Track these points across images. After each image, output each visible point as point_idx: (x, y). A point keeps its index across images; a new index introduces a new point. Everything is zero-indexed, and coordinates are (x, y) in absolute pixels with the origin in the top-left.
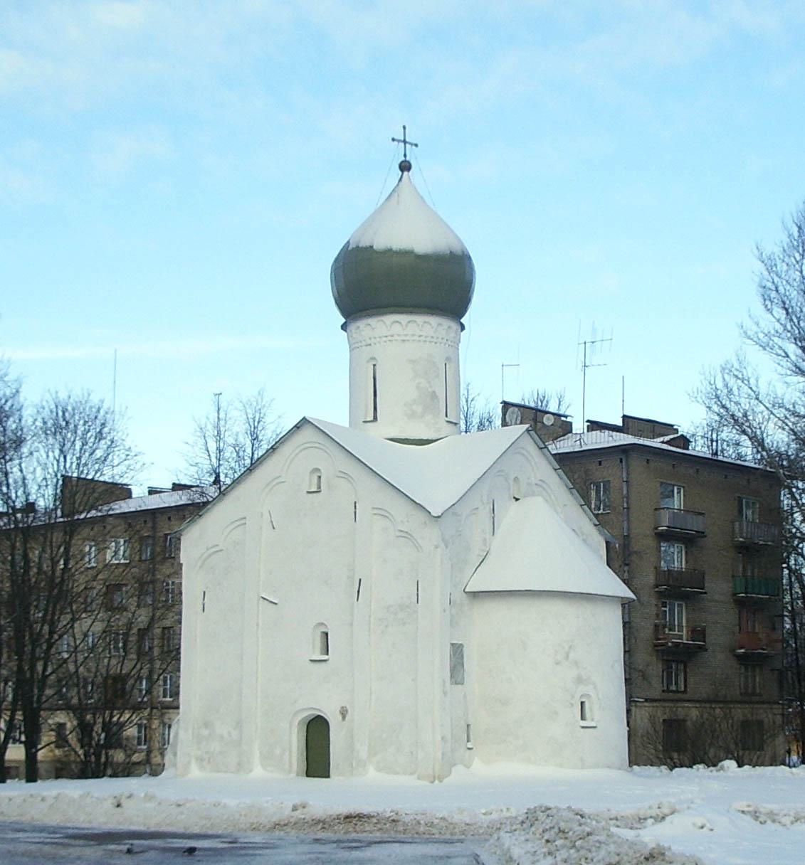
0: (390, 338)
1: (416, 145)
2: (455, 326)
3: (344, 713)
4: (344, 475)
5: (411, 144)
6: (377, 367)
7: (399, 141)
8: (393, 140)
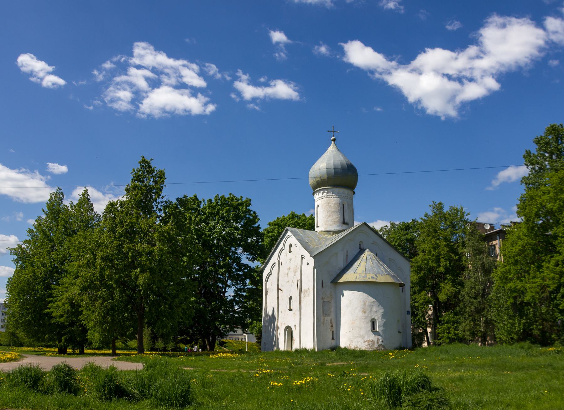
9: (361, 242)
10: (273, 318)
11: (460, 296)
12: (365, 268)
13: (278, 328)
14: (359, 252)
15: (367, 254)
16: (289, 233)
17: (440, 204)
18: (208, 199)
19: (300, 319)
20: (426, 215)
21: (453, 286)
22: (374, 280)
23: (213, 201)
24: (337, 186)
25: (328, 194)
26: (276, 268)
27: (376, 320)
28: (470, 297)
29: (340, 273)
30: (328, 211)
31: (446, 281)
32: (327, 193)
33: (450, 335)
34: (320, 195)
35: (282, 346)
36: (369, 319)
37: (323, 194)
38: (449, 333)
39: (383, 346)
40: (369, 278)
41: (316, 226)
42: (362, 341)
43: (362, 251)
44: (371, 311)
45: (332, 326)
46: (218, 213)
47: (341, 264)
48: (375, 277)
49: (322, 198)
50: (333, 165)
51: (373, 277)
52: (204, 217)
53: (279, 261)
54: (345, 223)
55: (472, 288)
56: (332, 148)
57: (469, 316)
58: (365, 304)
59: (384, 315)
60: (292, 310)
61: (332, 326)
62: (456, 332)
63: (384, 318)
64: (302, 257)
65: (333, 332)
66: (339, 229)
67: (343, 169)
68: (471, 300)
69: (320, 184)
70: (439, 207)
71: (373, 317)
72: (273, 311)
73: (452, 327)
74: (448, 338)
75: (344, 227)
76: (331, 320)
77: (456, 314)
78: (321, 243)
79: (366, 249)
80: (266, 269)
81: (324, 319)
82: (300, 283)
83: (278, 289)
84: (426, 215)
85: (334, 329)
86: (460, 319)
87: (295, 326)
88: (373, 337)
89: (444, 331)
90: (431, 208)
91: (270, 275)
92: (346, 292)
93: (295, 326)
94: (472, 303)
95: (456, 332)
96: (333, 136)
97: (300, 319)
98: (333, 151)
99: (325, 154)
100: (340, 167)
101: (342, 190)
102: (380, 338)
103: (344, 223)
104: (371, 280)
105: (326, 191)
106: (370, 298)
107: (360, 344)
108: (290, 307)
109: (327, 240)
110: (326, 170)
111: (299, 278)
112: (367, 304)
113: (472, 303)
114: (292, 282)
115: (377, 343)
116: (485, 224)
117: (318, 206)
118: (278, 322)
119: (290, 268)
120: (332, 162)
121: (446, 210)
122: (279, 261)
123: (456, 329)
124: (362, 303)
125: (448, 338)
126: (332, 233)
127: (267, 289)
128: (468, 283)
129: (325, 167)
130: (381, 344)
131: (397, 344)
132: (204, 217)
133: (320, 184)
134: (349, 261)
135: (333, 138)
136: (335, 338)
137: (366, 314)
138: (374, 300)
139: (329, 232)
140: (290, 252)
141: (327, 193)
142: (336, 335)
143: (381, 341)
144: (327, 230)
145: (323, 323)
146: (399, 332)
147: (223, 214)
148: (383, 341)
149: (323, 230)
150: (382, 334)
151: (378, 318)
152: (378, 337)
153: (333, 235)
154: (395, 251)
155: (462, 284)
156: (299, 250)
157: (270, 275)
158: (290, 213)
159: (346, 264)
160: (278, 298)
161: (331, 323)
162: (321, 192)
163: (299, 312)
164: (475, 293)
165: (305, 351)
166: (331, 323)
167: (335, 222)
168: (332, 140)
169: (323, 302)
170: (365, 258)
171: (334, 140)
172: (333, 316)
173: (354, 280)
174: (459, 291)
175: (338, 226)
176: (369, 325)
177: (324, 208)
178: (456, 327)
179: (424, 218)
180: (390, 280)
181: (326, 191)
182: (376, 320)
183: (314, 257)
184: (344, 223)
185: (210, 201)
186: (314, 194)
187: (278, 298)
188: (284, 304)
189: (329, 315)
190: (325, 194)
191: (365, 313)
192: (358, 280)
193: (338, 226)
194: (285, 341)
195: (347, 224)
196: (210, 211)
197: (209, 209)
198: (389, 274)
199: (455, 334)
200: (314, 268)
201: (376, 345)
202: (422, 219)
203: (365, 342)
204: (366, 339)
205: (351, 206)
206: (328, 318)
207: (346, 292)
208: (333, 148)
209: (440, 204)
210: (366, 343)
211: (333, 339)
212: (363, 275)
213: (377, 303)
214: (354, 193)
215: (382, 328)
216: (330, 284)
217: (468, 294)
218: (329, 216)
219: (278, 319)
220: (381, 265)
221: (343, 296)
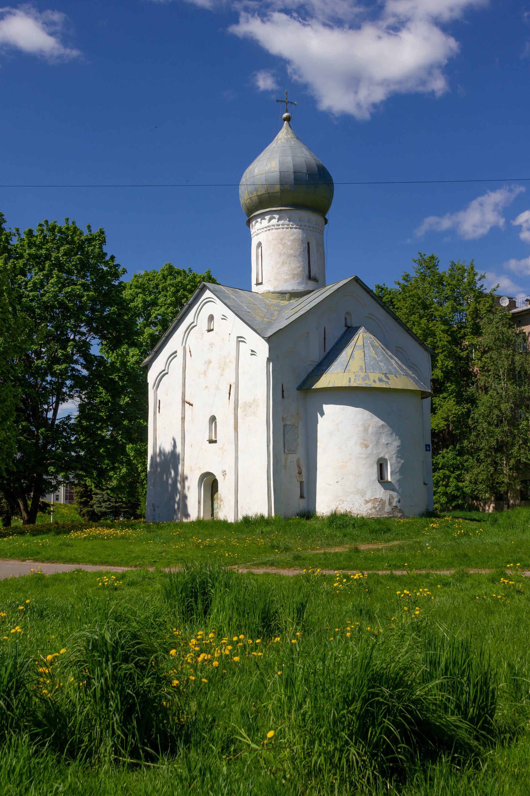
9: (348, 313)
10: (172, 460)
11: (470, 422)
12: (357, 363)
13: (184, 479)
14: (345, 333)
15: (361, 337)
16: (208, 294)
17: (432, 257)
18: (27, 230)
19: (237, 458)
20: (407, 278)
21: (458, 403)
22: (384, 386)
23: (36, 233)
24: (297, 206)
25: (281, 222)
26: (178, 361)
27: (386, 460)
28: (489, 423)
29: (313, 371)
30: (280, 255)
31: (445, 395)
32: (279, 219)
33: (449, 490)
34: (265, 223)
35: (195, 510)
36: (375, 459)
37: (270, 220)
38: (447, 486)
39: (401, 511)
40: (374, 380)
41: (254, 281)
42: (362, 501)
43: (349, 332)
44: (378, 443)
45: (300, 473)
46: (48, 257)
47: (316, 356)
48: (384, 379)
49: (268, 228)
50: (291, 166)
51: (380, 380)
52: (21, 262)
53: (185, 348)
54: (313, 277)
55: (490, 409)
56: (284, 135)
57: (486, 457)
58: (366, 430)
59: (401, 452)
60: (215, 442)
61: (300, 473)
62: (460, 484)
63: (401, 458)
64: (240, 339)
65: (301, 483)
66: (301, 288)
67: (310, 173)
68: (491, 428)
69: (267, 201)
70: (429, 264)
71: (382, 455)
72: (175, 446)
73: (453, 475)
74: (445, 494)
75: (311, 285)
76: (298, 461)
77: (461, 453)
78: (272, 315)
79: (357, 329)
80: (155, 364)
81: (286, 459)
82: (233, 390)
83: (184, 402)
84: (407, 278)
85: (304, 479)
86: (467, 461)
87: (224, 473)
88: (380, 493)
89: (438, 482)
90: (416, 265)
91: (163, 374)
92: (327, 408)
93: (224, 473)
94: (491, 434)
95: (460, 484)
96: (287, 112)
97: (237, 458)
98: (287, 140)
99: (273, 145)
100: (305, 170)
101: (306, 215)
102: (395, 494)
103: (310, 278)
104: (378, 385)
105: (277, 216)
106: (376, 419)
107: (357, 505)
108: (210, 435)
109: (282, 309)
110: (278, 173)
111: (233, 381)
112: (370, 430)
113: (491, 434)
114: (217, 388)
115: (390, 503)
116: (500, 297)
117: (260, 245)
118: (183, 465)
119: (210, 362)
120: (290, 159)
121: (443, 269)
122: (185, 348)
123: (459, 478)
124: (361, 429)
125: (445, 494)
126: (287, 296)
127: (158, 405)
128: (484, 399)
129: (277, 169)
130: (396, 507)
131: (422, 508)
132: (21, 262)
133: (267, 201)
134: (328, 349)
135: (285, 115)
136: (305, 495)
137: (369, 450)
138: (383, 423)
139: (282, 294)
140: (209, 330)
141: (279, 219)
142: (308, 489)
143: (396, 500)
144: (279, 289)
145: (285, 467)
146: (425, 484)
147: (57, 258)
148: (399, 501)
149: (271, 289)
150: (397, 487)
151: (391, 458)
152: (391, 492)
153: (290, 299)
154: (406, 333)
155: (472, 401)
156: (232, 325)
157: (163, 374)
158: (164, 266)
159: (323, 354)
160: (183, 419)
161: (299, 467)
162: (267, 217)
163: (233, 446)
164: (498, 416)
165: (261, 521)
166: (299, 467)
167: (294, 276)
168: (285, 120)
169: (285, 426)
170: (360, 343)
171: (288, 119)
172: (300, 453)
173: (344, 383)
174: (468, 414)
175: (300, 283)
176: (375, 470)
177: (272, 249)
178: (459, 475)
179: (402, 282)
180: (411, 385)
181: (277, 216)
182: (386, 460)
183: (268, 340)
184: (310, 278)
185: (30, 233)
186: (249, 222)
187: (183, 419)
188: (198, 431)
189: (294, 452)
190: (274, 221)
191: (367, 447)
192: (355, 385)
193: (300, 283)
194: (199, 502)
195: (315, 280)
196: (33, 251)
197: (30, 247)
198: (407, 375)
199: (458, 489)
200: (269, 360)
201: (387, 508)
202: (399, 284)
203: (367, 502)
204: (368, 496)
205: (321, 245)
206: (292, 458)
207: (327, 408)
208: (287, 133)
209: (432, 257)
210: (370, 505)
211: (302, 497)
212: (363, 375)
213: (387, 429)
214: (326, 221)
215: (398, 477)
216: (297, 391)
217: (485, 417)
218: (283, 263)
219: (183, 460)
220: (392, 358)
221: (322, 414)
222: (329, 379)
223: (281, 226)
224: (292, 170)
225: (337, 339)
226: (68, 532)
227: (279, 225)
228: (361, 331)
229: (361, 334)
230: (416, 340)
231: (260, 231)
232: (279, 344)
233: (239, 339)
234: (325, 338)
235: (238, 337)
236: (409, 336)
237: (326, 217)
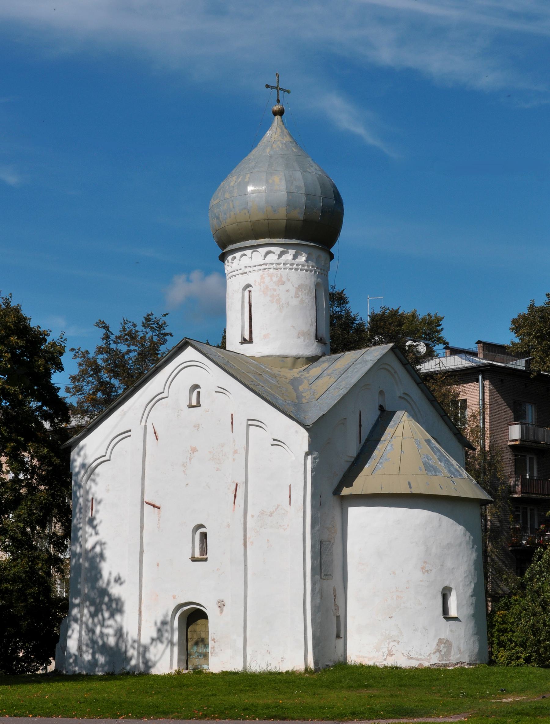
0: (264, 267)
1: (288, 92)
2: (324, 256)
3: (221, 605)
4: (222, 390)
5: (284, 91)
6: (253, 294)
7: (272, 87)
8: (267, 86)
26: (133, 443)
43: (385, 417)
83: (142, 502)
111: (241, 480)
186: (223, 258)
190: (273, 258)
214: (332, 257)
222: (362, 484)
223: (282, 265)
224: (303, 191)
225: (371, 426)
226: (296, 720)
227: (279, 264)
228: (399, 414)
229: (407, 422)
230: (450, 429)
231: (250, 269)
232: (320, 433)
233: (250, 422)
234: (360, 426)
235: (249, 420)
236: (443, 424)
237: (332, 250)
